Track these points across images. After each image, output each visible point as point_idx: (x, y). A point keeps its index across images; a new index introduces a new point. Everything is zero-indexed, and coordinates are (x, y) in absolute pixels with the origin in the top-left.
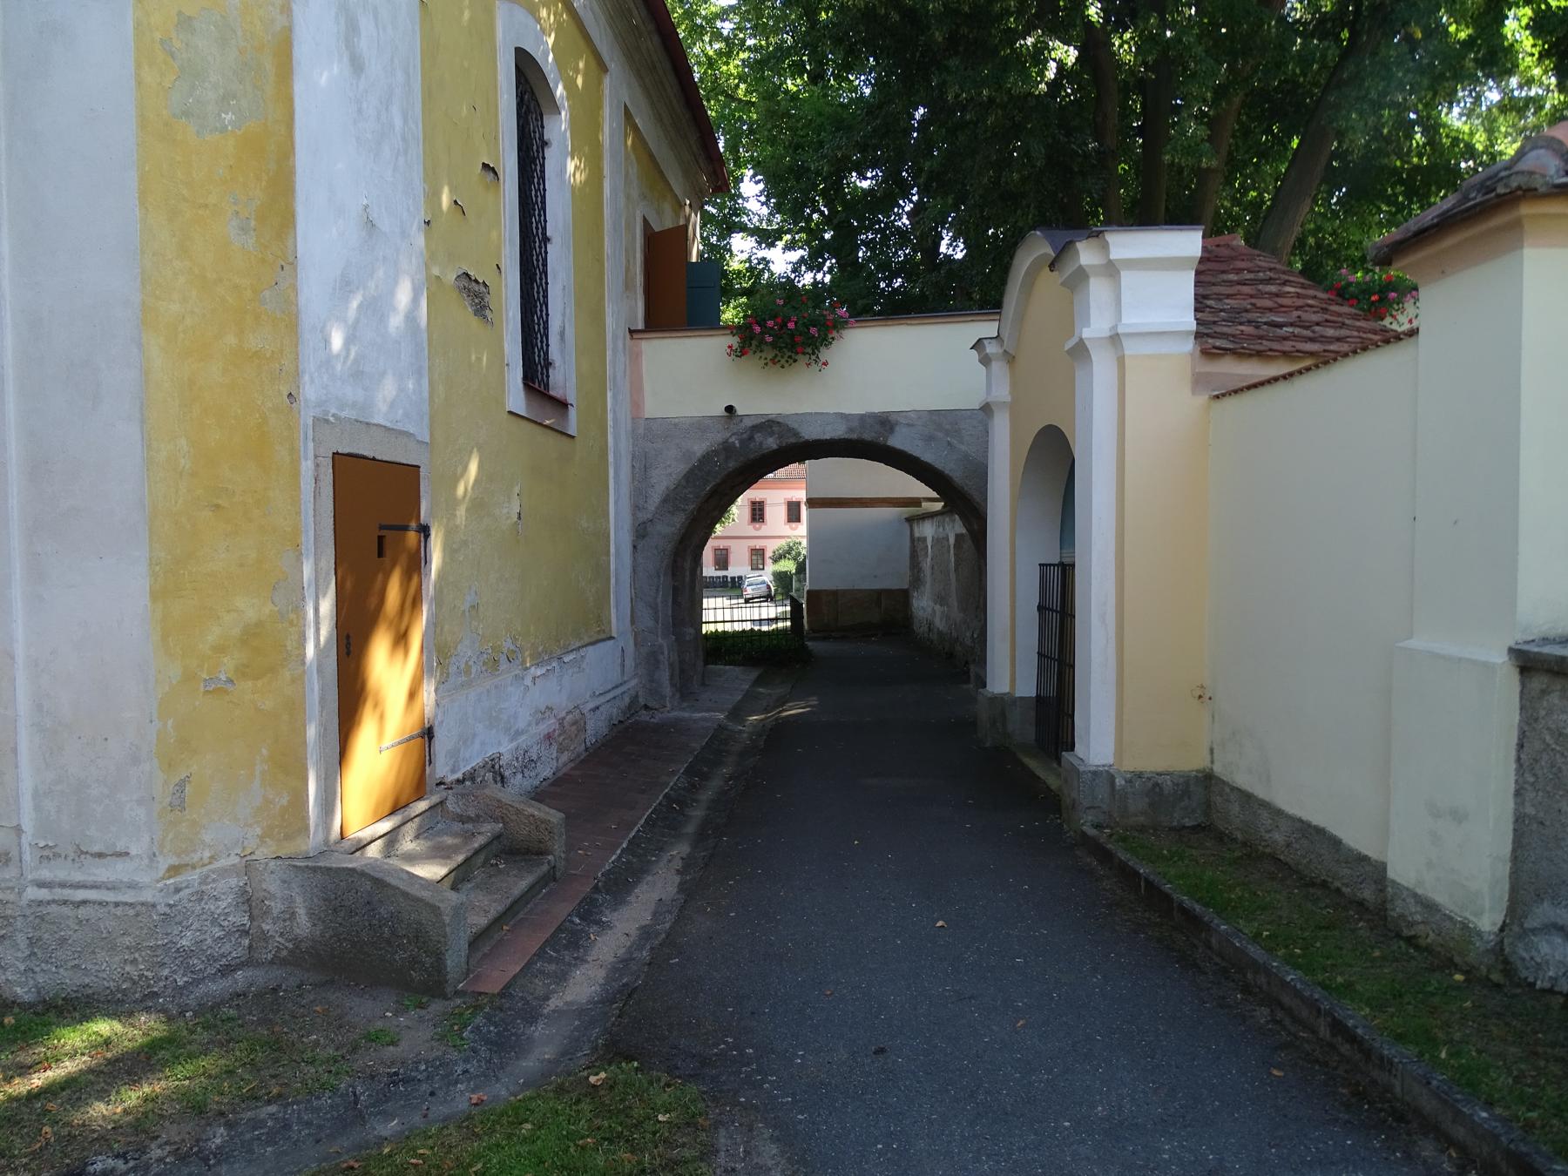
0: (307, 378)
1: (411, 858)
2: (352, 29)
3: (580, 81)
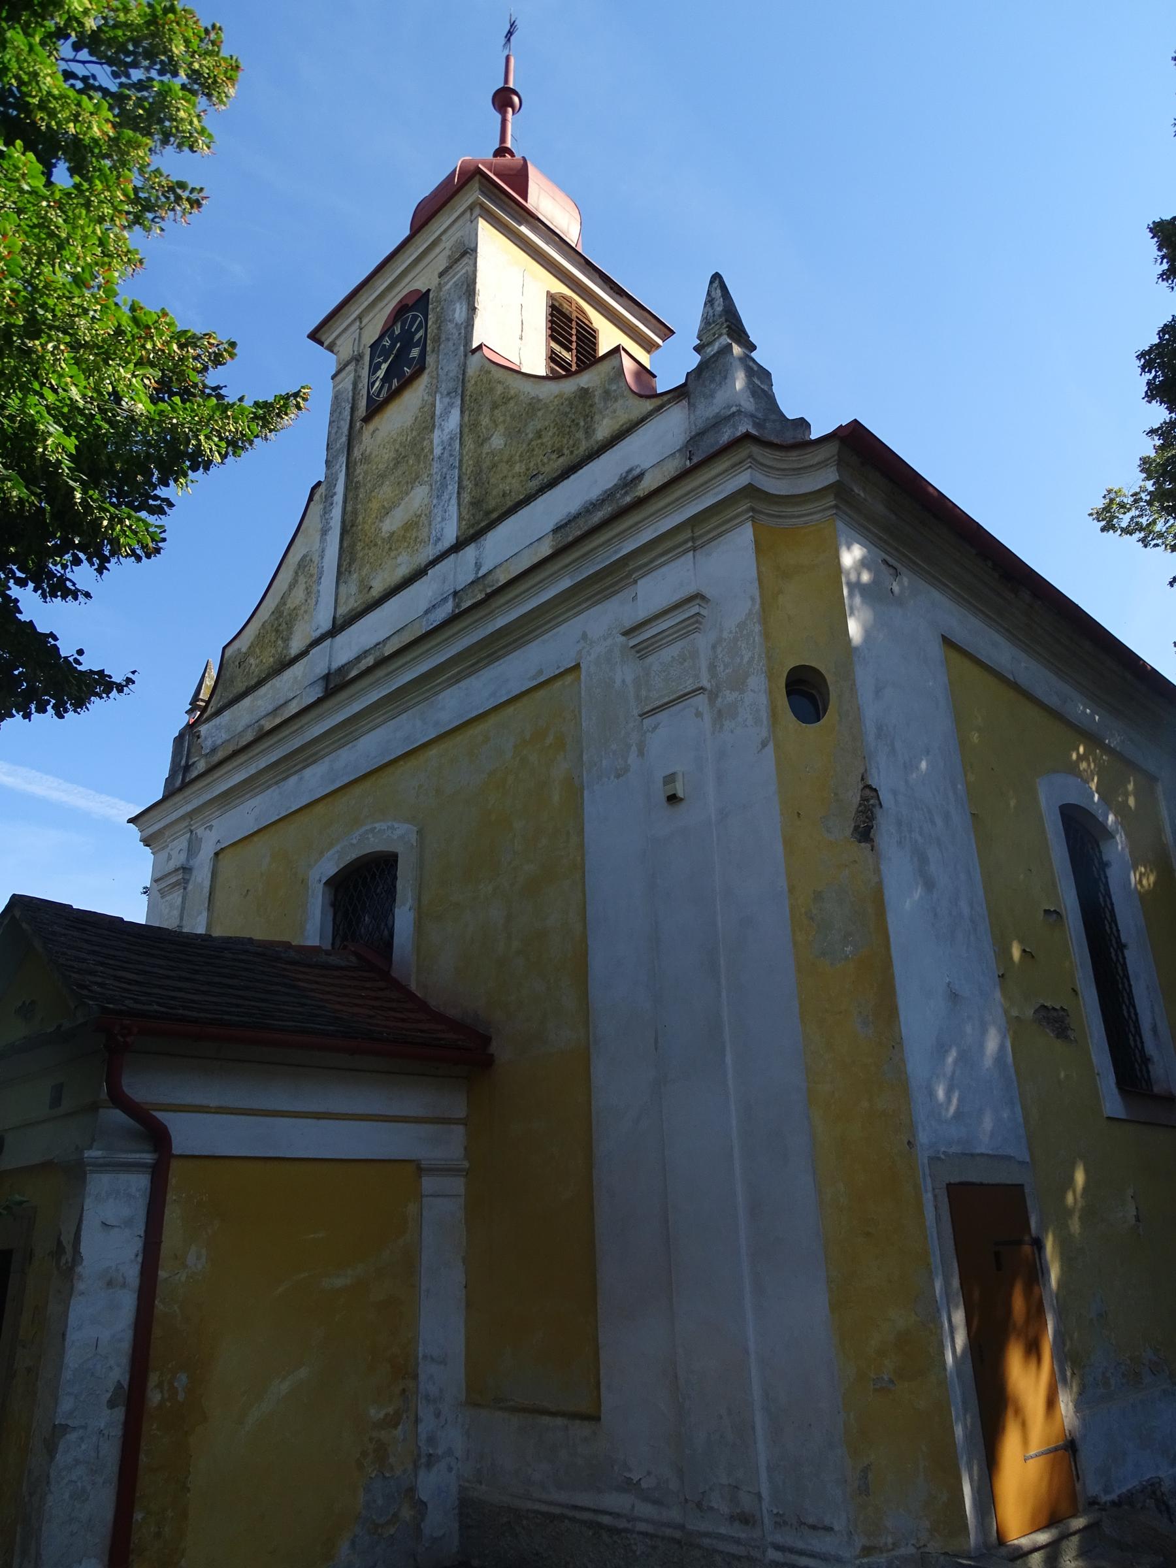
0: (920, 1128)
3: (1131, 801)
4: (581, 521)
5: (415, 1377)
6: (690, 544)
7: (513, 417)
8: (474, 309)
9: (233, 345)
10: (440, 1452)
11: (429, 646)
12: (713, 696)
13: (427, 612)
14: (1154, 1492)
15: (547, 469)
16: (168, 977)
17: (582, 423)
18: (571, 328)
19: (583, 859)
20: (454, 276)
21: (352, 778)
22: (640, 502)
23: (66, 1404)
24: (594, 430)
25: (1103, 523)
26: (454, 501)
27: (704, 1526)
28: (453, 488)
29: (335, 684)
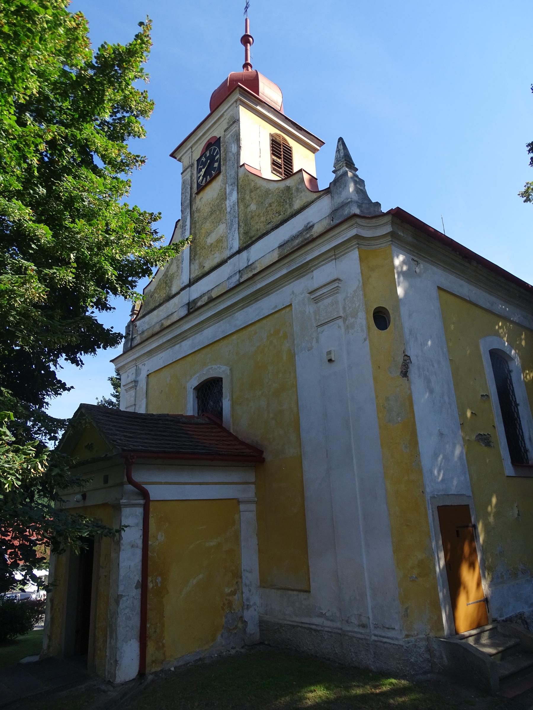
1: (484, 646)
3: (523, 343)
4: (289, 244)
5: (241, 577)
6: (334, 257)
7: (259, 196)
8: (240, 147)
9: (160, 214)
10: (251, 604)
11: (230, 295)
12: (345, 320)
13: (228, 279)
14: (521, 617)
15: (274, 220)
17: (288, 202)
18: (281, 149)
19: (296, 383)
20: (230, 132)
21: (202, 347)
22: (314, 240)
23: (121, 588)
24: (293, 205)
25: (525, 198)
26: (237, 232)
27: (348, 629)
28: (236, 226)
29: (192, 308)
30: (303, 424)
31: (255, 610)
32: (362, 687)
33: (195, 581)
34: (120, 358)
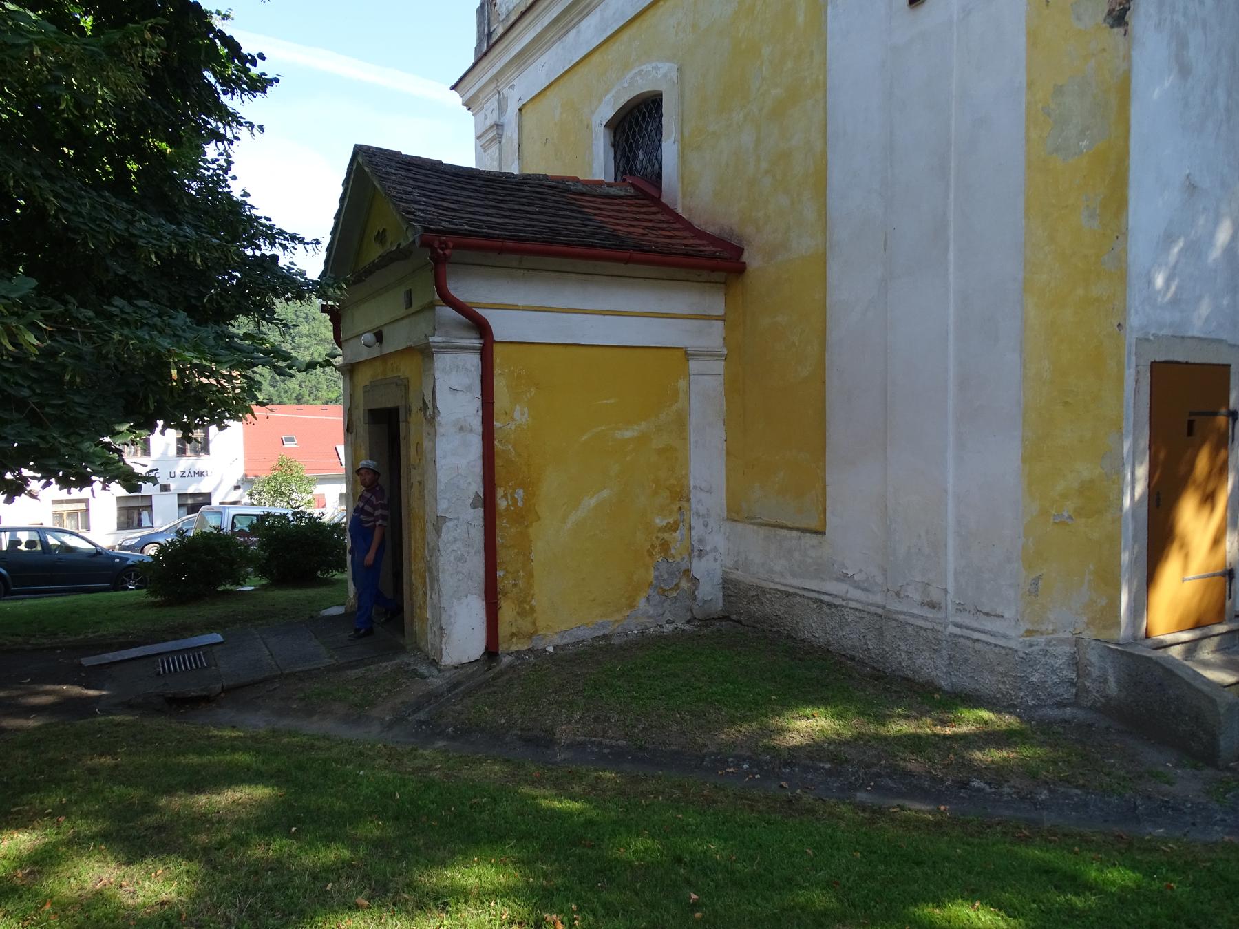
0: (1132, 311)
1: (1206, 665)
2: (1182, 43)
5: (689, 500)
10: (708, 548)
16: (477, 205)
23: (443, 506)
27: (899, 607)
30: (836, 177)
31: (716, 560)
32: (916, 718)
33: (593, 502)
34: (468, 78)
